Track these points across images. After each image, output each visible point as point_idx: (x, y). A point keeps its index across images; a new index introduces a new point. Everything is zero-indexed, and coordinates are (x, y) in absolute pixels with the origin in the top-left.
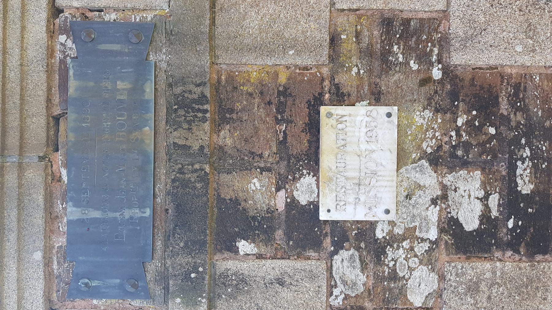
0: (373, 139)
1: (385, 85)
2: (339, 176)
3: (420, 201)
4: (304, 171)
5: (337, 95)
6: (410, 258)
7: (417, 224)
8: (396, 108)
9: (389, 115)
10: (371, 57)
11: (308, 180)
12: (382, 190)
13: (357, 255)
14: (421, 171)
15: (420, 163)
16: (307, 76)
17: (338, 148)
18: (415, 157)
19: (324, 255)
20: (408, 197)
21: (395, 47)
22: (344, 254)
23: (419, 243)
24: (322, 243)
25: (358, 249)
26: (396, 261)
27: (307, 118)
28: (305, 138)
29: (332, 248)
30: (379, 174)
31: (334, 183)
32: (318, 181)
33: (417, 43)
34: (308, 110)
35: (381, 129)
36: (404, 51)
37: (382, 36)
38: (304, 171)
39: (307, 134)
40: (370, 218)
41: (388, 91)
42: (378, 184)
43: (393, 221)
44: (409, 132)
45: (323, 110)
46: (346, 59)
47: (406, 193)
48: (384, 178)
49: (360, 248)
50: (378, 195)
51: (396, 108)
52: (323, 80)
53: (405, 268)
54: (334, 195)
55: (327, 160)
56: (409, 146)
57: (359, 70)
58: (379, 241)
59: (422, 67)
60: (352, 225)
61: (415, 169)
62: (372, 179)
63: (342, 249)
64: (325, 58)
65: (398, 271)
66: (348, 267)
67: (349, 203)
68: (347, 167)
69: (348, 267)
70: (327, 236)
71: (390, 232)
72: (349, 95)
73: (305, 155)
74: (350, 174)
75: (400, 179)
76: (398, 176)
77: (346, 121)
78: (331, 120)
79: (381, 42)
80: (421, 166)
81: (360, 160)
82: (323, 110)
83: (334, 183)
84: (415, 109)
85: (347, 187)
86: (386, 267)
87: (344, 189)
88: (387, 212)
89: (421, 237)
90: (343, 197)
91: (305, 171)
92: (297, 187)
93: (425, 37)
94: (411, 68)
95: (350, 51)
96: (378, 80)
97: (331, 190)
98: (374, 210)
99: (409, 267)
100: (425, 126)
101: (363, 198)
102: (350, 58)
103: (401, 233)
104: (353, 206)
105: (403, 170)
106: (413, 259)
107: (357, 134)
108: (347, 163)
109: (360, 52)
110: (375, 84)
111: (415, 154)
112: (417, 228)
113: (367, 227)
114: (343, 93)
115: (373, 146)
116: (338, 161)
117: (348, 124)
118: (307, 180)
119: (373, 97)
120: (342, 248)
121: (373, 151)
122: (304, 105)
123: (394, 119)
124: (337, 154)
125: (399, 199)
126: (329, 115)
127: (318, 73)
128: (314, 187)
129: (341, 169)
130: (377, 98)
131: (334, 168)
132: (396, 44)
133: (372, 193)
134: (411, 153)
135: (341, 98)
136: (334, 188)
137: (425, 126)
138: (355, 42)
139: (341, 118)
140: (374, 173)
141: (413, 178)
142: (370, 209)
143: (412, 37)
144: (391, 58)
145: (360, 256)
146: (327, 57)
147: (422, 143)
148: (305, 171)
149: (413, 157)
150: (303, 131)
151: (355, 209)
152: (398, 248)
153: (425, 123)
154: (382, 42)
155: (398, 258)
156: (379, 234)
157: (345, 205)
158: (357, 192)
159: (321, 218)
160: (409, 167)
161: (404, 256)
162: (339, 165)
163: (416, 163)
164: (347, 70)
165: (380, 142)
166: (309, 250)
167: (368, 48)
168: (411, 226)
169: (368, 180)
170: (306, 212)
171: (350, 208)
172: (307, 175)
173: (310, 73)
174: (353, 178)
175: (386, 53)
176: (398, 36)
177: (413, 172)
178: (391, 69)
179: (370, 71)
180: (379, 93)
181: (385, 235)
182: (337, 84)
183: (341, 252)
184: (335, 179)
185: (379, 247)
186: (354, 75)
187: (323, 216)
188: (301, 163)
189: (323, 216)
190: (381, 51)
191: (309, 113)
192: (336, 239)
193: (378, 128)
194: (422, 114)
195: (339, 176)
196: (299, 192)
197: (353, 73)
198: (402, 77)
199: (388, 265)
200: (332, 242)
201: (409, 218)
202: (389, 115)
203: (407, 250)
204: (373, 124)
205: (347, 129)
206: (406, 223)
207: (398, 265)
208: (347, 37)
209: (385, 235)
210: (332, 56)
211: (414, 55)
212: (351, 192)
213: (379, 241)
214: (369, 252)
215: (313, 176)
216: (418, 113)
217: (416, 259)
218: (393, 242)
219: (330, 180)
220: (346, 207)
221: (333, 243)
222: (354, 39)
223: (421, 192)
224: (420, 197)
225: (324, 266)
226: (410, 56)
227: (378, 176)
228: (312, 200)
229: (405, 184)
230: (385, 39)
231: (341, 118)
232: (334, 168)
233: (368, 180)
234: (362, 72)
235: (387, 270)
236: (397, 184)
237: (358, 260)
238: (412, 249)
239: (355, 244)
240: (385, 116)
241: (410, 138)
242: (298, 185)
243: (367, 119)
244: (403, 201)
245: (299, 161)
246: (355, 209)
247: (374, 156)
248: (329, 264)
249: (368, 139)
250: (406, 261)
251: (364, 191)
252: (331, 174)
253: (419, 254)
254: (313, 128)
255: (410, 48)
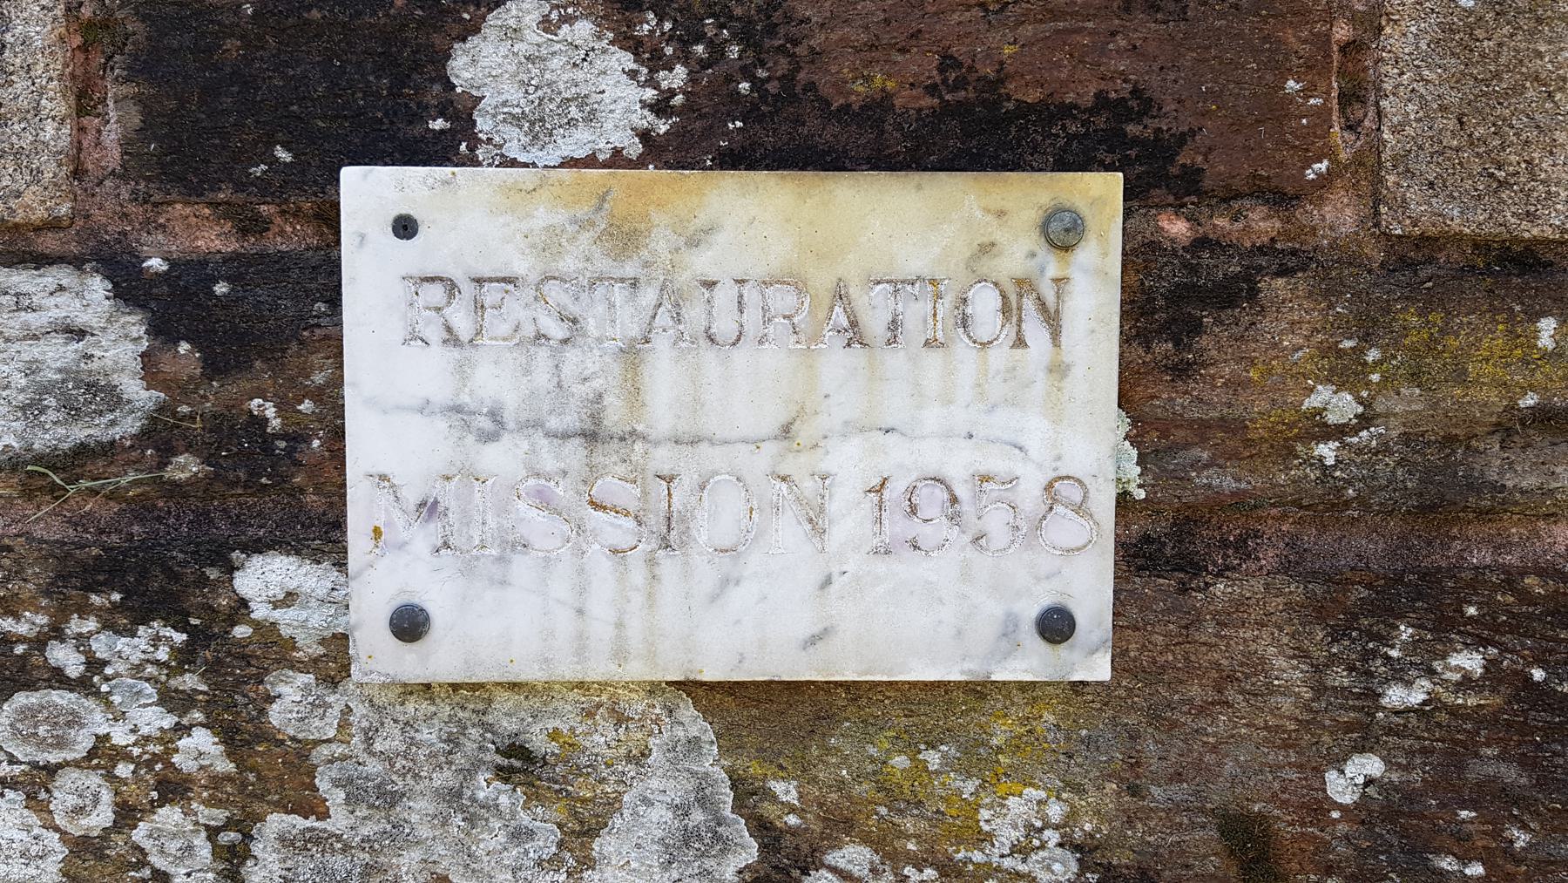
0: (897, 526)
1: (1240, 604)
2: (649, 296)
3: (491, 839)
4: (680, 71)
5: (1179, 295)
6: (110, 777)
7: (339, 821)
8: (1100, 669)
9: (1056, 626)
10: (1424, 510)
11: (620, 98)
12: (561, 588)
13: (116, 432)
14: (688, 837)
15: (739, 829)
16: (1307, 92)
17: (840, 295)
18: (774, 798)
19: (111, 207)
20: (518, 763)
21: (1470, 662)
22: (120, 345)
23: (212, 833)
24: (193, 192)
25: (161, 435)
26: (83, 685)
27: (1033, 96)
28: (903, 80)
29: (156, 264)
30: (669, 566)
31: (603, 264)
32: (617, 160)
33: (1499, 802)
34: (1088, 100)
35: (966, 575)
36: (1443, 717)
37: (1541, 572)
38: (680, 71)
39: (932, 90)
40: (362, 509)
41: (1198, 621)
42: (601, 565)
43: (345, 669)
44: (933, 759)
45: (1100, 193)
46: (1412, 349)
47: (538, 742)
48: (638, 599)
49: (166, 452)
50: (521, 566)
51: (1100, 669)
52: (1282, 198)
53: (41, 744)
54: (520, 266)
55: (752, 219)
56: (846, 756)
57: (1339, 432)
58: (213, 573)
59: (1342, 828)
60: (318, 395)
61: (703, 801)
62: (629, 523)
63: (155, 330)
64: (1419, 207)
65: (21, 699)
66: (31, 369)
67: (462, 371)
68: (709, 356)
69: (31, 369)
70: (244, 232)
71: (275, 649)
72: (1181, 371)
73: (788, 80)
74: (664, 372)
75: (637, 705)
76: (653, 689)
77: (1020, 342)
78: (1030, 240)
79: (1505, 569)
80: (717, 837)
81: (757, 442)
82: (1100, 193)
83: (603, 264)
84: (1079, 790)
85: (571, 355)
86: (42, 619)
87: (557, 331)
88: (409, 625)
89: (257, 848)
90: (505, 329)
91: (676, 77)
92: (568, 20)
93: (1521, 839)
94: (1339, 763)
95: (1461, 377)
96: (1269, 558)
97: (549, 244)
98: (423, 538)
99: (52, 770)
100: (978, 857)
101: (502, 459)
102: (1415, 377)
103: (276, 715)
104: (441, 390)
105: (692, 721)
106: (106, 797)
107: (932, 417)
108: (740, 356)
109: (1450, 440)
110: (1241, 542)
111: (792, 797)
112: (312, 822)
113: (310, 498)
114: (1197, 328)
115: (850, 518)
116: (751, 294)
117: (1001, 355)
118: (620, 96)
119: (1161, 527)
120: (163, 331)
121: (816, 523)
122: (1121, 69)
123: (1031, 663)
124: (799, 285)
125: (505, 702)
126: (1063, 233)
127: (1323, 166)
128: (577, 142)
129: (694, 314)
130: (1161, 550)
131: (702, 262)
132: (1490, 665)
133: (534, 522)
134: (803, 772)
135: (1169, 314)
136: (569, 264)
137: (978, 857)
138: (1512, 408)
139: (1042, 305)
140: (670, 534)
141: (638, 787)
142: (429, 509)
143: (1524, 762)
144: (1406, 632)
145: (108, 450)
146: (1427, 226)
147: (866, 840)
148: (676, 77)
149: (778, 787)
150: (948, 62)
151: (425, 408)
152: (170, 700)
153: (996, 854)
154: (1511, 579)
155: (105, 700)
156: (262, 579)
157: (451, 338)
158: (537, 424)
159: (350, 176)
160: (711, 763)
161: (120, 737)
162: (724, 296)
163: (738, 807)
164: (1341, 353)
165: (881, 566)
166: (138, 99)
167: (1475, 486)
168: (323, 784)
169: (627, 495)
170: (400, 81)
171: (430, 372)
172: (650, 94)
173: (1322, 114)
174: (634, 393)
175: (1434, 603)
176: (1538, 674)
177: (679, 789)
178: (1336, 636)
179: (1327, 504)
180: (1190, 567)
181: (260, 612)
182: (1253, 293)
183: (135, 324)
184: (630, 270)
185: (175, 577)
186: (1313, 401)
187: (367, 193)
188: (734, 51)
189: (367, 193)
190: (1452, 571)
191: (1067, 111)
192: (221, 288)
193: (971, 552)
194: (1052, 837)
195: (649, 296)
196: (534, 36)
197: (1321, 396)
198: (1286, 704)
199: (56, 632)
200: (203, 263)
201: (374, 767)
202: (1056, 626)
203: (165, 758)
204: (996, 522)
205: (963, 349)
206: (339, 750)
207: (61, 698)
208: (1546, 355)
209: (260, 612)
210: (1430, 260)
211: (1416, 776)
212: (542, 377)
213: (213, 573)
214: (141, 509)
215: (645, 136)
216: (1055, 811)
217: (102, 817)
218: (213, 671)
219: (624, 238)
220: (436, 348)
221: (191, 274)
222: (1530, 400)
223: (546, 840)
224: (520, 835)
225: (33, 205)
226: (1411, 753)
227: (651, 562)
228: (483, 124)
229: (601, 739)
230: (1525, 596)
231: (1042, 305)
232: (702, 262)
233: (627, 495)
234: (1327, 451)
235: (23, 629)
236: (603, 686)
237: (79, 433)
238: (173, 788)
239: (192, 418)
240: (1046, 601)
241: (900, 761)
242: (583, 29)
243: (1030, 494)
244: (487, 727)
245: (745, 37)
246: (425, 408)
247: (788, 531)
248: (49, 243)
249: (895, 491)
250: (92, 754)
251: (549, 464)
252: (660, 243)
253: (139, 834)
254: (972, 133)
255: (1459, 753)
